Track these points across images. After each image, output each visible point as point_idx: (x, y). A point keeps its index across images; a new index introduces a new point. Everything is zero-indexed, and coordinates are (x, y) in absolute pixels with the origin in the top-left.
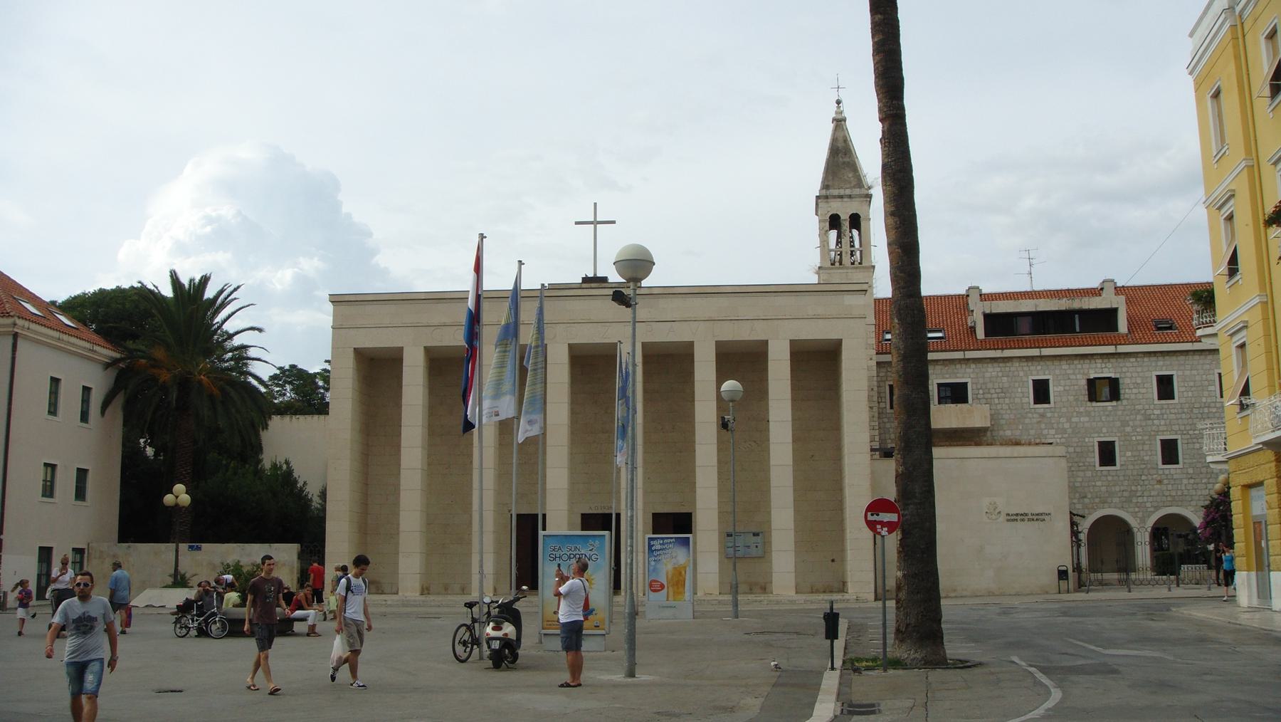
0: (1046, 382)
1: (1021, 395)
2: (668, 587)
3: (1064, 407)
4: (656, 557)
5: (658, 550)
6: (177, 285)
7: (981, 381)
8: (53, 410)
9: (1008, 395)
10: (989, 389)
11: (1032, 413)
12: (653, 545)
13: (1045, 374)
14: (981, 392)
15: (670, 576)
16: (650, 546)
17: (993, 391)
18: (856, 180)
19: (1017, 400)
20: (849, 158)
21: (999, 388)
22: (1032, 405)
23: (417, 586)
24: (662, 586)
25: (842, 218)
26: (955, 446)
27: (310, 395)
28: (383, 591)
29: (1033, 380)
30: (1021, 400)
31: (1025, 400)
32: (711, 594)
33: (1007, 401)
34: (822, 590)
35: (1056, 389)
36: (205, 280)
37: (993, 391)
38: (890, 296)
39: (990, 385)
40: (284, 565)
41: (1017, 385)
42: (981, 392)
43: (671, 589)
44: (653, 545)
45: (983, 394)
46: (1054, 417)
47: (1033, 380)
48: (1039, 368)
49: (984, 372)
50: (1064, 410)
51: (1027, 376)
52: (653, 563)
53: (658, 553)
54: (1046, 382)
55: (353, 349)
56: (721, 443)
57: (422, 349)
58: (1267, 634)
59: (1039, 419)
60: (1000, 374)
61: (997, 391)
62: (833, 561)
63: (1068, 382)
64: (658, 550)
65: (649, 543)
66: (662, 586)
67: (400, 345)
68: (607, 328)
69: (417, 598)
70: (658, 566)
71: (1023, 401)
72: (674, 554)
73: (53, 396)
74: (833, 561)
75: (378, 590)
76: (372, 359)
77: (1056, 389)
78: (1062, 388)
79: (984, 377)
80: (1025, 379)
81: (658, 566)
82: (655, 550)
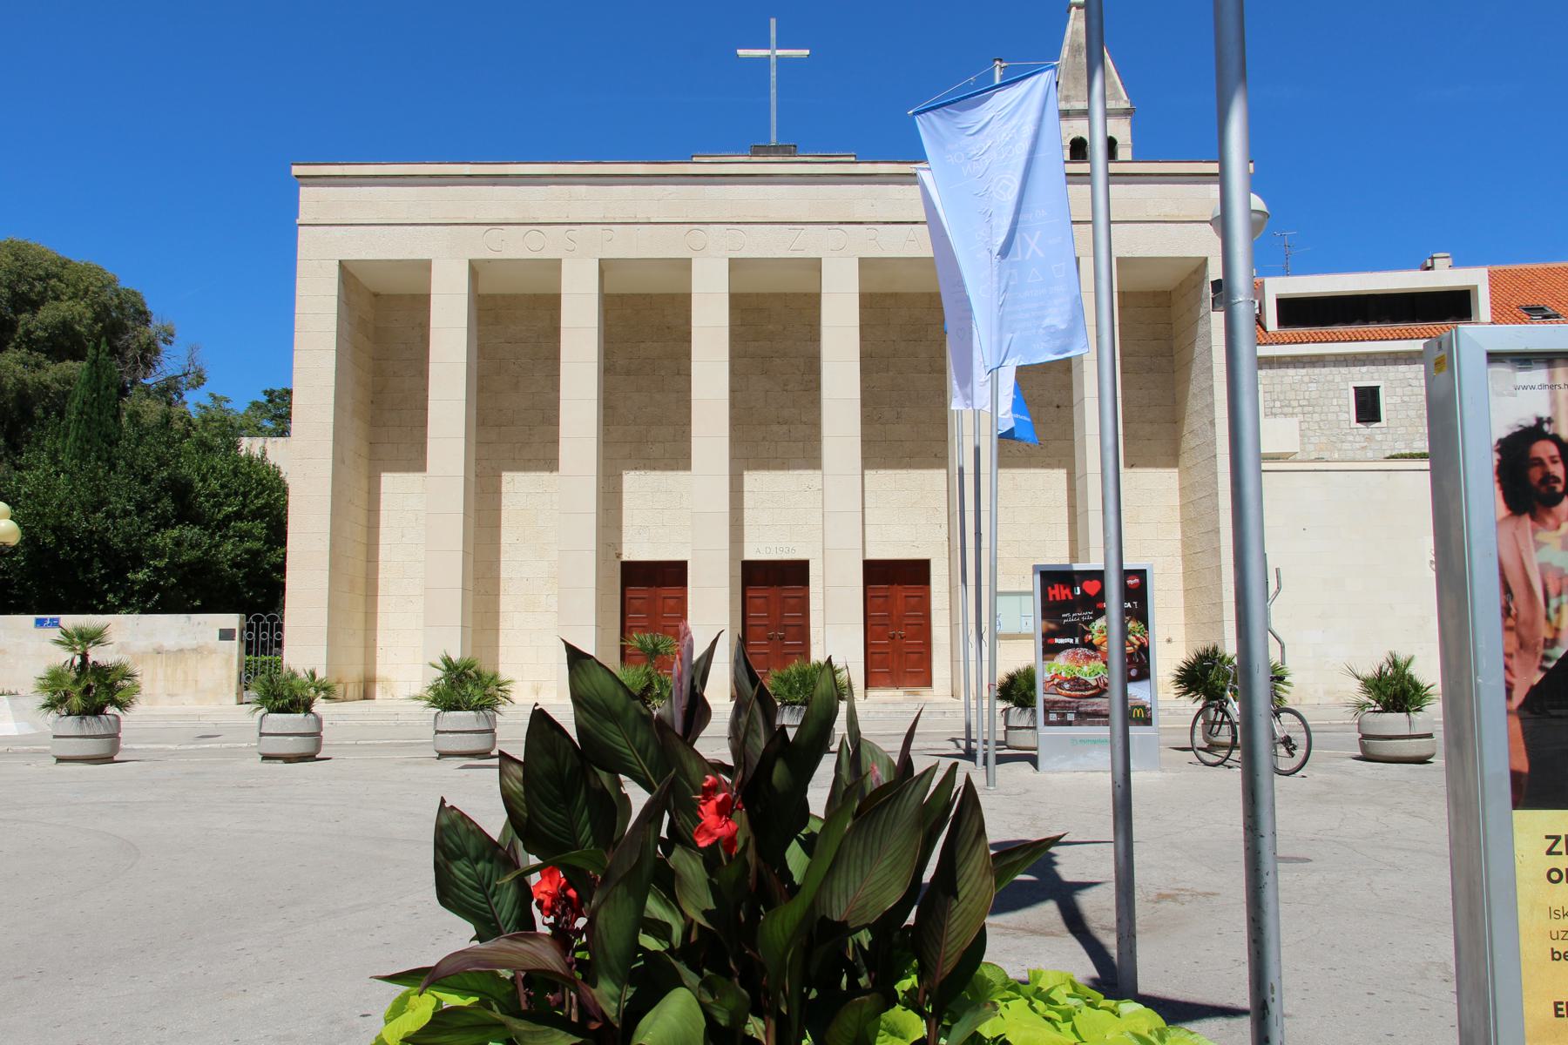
0: (1374, 391)
1: (1337, 409)
6: (581, 700)
7: (1278, 388)
8: (1277, 570)
9: (1318, 409)
10: (1290, 400)
13: (1373, 379)
14: (1278, 404)
17: (1295, 404)
19: (1331, 417)
21: (1304, 399)
25: (1119, 143)
27: (37, 445)
29: (1355, 388)
30: (1337, 416)
31: (1344, 416)
33: (1316, 417)
35: (1389, 400)
36: (575, 657)
37: (1295, 404)
38: (383, 474)
39: (1291, 395)
41: (1331, 394)
42: (1278, 404)
45: (1281, 407)
46: (1386, 441)
47: (1355, 388)
49: (1282, 377)
50: (1402, 430)
51: (1346, 381)
54: (1374, 391)
56: (1137, 467)
59: (1366, 444)
60: (1306, 379)
61: (1302, 403)
63: (1408, 390)
73: (292, 760)
74: (1169, 641)
76: (376, 295)
77: (1389, 400)
79: (1282, 383)
80: (1342, 386)
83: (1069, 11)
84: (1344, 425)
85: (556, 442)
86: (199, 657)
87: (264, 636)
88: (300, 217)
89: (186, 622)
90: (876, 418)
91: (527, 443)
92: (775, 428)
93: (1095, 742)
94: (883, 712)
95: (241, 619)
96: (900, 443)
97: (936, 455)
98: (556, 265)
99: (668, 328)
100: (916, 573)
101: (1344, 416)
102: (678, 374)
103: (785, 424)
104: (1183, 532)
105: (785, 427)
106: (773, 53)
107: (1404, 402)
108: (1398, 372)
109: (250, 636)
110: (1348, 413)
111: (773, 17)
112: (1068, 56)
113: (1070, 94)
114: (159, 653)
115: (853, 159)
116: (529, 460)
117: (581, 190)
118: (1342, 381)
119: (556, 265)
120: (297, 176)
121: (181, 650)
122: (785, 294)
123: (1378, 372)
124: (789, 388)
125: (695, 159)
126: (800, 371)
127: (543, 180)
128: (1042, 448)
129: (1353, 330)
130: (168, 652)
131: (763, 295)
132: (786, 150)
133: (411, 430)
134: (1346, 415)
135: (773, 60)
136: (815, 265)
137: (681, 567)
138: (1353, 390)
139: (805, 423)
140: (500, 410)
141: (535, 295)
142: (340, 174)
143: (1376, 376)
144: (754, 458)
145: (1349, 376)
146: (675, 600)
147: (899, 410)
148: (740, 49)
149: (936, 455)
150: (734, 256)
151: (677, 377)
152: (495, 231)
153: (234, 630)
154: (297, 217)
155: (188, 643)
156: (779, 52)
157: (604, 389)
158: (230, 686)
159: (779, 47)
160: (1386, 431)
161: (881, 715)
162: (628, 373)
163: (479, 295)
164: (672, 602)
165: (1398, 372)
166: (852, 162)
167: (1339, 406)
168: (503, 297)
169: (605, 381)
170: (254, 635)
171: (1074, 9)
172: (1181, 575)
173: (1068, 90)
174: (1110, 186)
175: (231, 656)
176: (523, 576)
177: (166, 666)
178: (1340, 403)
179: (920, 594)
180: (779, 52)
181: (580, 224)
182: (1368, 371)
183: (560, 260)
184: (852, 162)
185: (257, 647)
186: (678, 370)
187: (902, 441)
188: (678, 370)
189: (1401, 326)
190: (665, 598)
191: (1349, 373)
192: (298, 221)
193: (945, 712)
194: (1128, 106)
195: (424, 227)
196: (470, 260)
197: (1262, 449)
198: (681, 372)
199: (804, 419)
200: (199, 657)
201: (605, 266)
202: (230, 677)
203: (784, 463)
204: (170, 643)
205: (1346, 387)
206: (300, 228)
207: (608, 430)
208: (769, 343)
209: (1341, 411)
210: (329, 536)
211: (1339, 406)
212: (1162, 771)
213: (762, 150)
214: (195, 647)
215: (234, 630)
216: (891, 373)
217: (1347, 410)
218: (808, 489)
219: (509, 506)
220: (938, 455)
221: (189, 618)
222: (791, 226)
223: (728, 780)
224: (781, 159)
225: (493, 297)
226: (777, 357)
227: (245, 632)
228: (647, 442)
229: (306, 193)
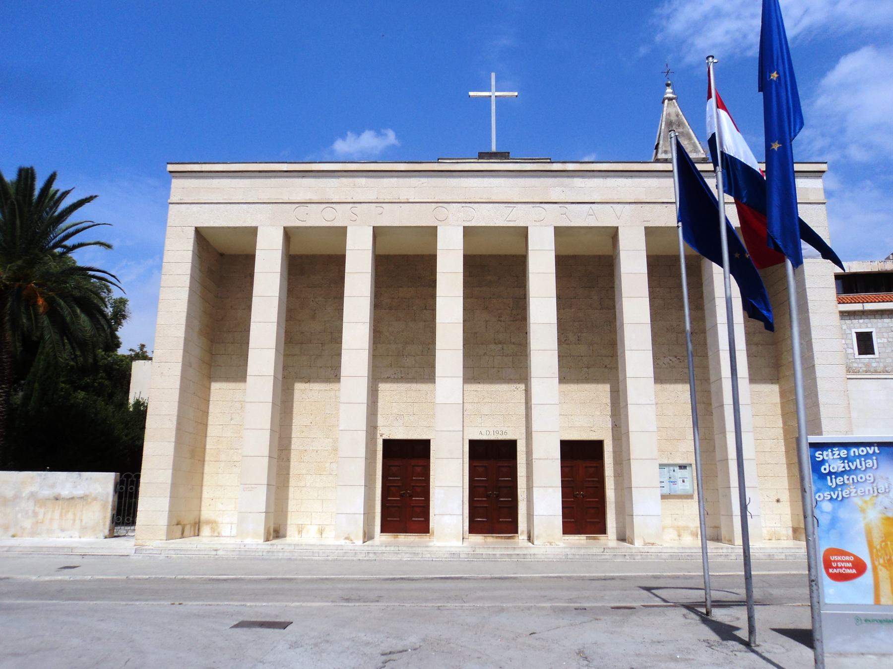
2: (875, 569)
3: (889, 357)
4: (834, 490)
5: (837, 474)
11: (857, 363)
12: (823, 462)
13: (867, 327)
15: (877, 542)
16: (816, 465)
18: (692, 146)
20: (683, 129)
22: (857, 356)
23: (261, 530)
24: (860, 567)
26: (63, 548)
28: (219, 533)
29: (856, 333)
30: (846, 351)
32: (653, 544)
34: (767, 538)
35: (879, 341)
40: (95, 499)
43: (883, 573)
44: (823, 462)
48: (861, 321)
52: (827, 506)
53: (839, 480)
55: (194, 229)
57: (283, 227)
58: (671, 555)
62: (778, 501)
64: (837, 474)
65: (813, 457)
66: (860, 567)
67: (254, 225)
68: (512, 208)
69: (260, 547)
70: (843, 514)
71: (848, 352)
72: (882, 485)
74: (778, 501)
75: (214, 532)
76: (222, 255)
77: (879, 341)
78: (885, 340)
80: (848, 331)
81: (843, 514)
82: (830, 473)
83: (663, 102)
84: (851, 357)
85: (340, 355)
86: (84, 503)
87: (131, 489)
88: (171, 198)
89: (77, 478)
90: (563, 341)
91: (320, 356)
92: (493, 346)
93: (881, 621)
94: (578, 555)
95: (116, 476)
96: (580, 358)
97: (606, 366)
98: (343, 231)
99: (419, 278)
100: (596, 447)
101: (850, 351)
102: (426, 309)
103: (500, 344)
104: (784, 423)
105: (500, 346)
106: (493, 94)
107: (890, 342)
108: (884, 322)
109: (121, 488)
110: (853, 349)
111: (493, 72)
112: (665, 127)
113: (667, 149)
114: (57, 499)
115: (549, 161)
116: (321, 367)
117: (362, 181)
118: (848, 329)
119: (343, 231)
120: (171, 172)
121: (73, 498)
122: (500, 256)
123: (870, 323)
124: (502, 319)
125: (440, 161)
126: (510, 307)
127: (336, 174)
128: (680, 362)
129: (851, 296)
130: (64, 499)
131: (484, 256)
132: (502, 156)
133: (241, 345)
134: (851, 350)
135: (493, 98)
136: (523, 232)
137: (424, 445)
138: (855, 334)
139: (514, 344)
140: (303, 333)
141: (329, 255)
142: (199, 170)
143: (869, 325)
144: (478, 367)
145: (852, 325)
146: (421, 468)
147: (579, 334)
148: (471, 91)
149: (606, 366)
150: (467, 224)
151: (425, 311)
152: (302, 208)
153: (820, 433)
154: (169, 199)
155: (79, 492)
156: (498, 94)
157: (374, 319)
158: (104, 525)
159: (496, 91)
160: (879, 361)
161: (577, 557)
162: (390, 308)
163: (290, 255)
164: (419, 469)
165: (884, 322)
166: (549, 162)
167: (847, 344)
168: (307, 256)
169: (374, 313)
170: (124, 489)
171: (666, 101)
172: (784, 452)
173: (665, 147)
174: (299, 387)
175: (107, 502)
176: (314, 448)
177: (62, 509)
178: (847, 342)
179: (595, 465)
180: (498, 94)
181: (361, 203)
182: (863, 322)
183: (347, 227)
184: (549, 162)
185: (126, 497)
186: (426, 307)
187: (582, 356)
188: (426, 307)
189: (882, 294)
190: (414, 466)
191: (852, 323)
192: (169, 201)
193: (625, 555)
194: (704, 156)
195: (253, 205)
196: (284, 228)
197: (688, 395)
198: (427, 308)
199: (513, 340)
200: (84, 503)
201: (378, 232)
202: (105, 517)
203: (499, 371)
204: (65, 493)
205: (850, 332)
206: (171, 205)
207: (376, 347)
208: (489, 288)
209: (848, 348)
210: (176, 417)
211: (847, 344)
212: (771, 594)
213: (485, 155)
214: (82, 496)
215: (820, 433)
216: (573, 310)
217: (852, 347)
218: (516, 390)
219: (306, 399)
220: (608, 366)
221: (80, 475)
222: (506, 205)
223: (387, 505)
224: (499, 161)
225: (301, 257)
226: (494, 298)
227: (118, 486)
228: (403, 356)
229: (176, 183)
